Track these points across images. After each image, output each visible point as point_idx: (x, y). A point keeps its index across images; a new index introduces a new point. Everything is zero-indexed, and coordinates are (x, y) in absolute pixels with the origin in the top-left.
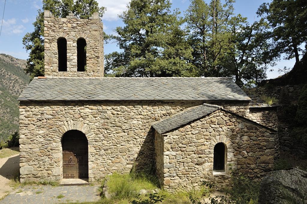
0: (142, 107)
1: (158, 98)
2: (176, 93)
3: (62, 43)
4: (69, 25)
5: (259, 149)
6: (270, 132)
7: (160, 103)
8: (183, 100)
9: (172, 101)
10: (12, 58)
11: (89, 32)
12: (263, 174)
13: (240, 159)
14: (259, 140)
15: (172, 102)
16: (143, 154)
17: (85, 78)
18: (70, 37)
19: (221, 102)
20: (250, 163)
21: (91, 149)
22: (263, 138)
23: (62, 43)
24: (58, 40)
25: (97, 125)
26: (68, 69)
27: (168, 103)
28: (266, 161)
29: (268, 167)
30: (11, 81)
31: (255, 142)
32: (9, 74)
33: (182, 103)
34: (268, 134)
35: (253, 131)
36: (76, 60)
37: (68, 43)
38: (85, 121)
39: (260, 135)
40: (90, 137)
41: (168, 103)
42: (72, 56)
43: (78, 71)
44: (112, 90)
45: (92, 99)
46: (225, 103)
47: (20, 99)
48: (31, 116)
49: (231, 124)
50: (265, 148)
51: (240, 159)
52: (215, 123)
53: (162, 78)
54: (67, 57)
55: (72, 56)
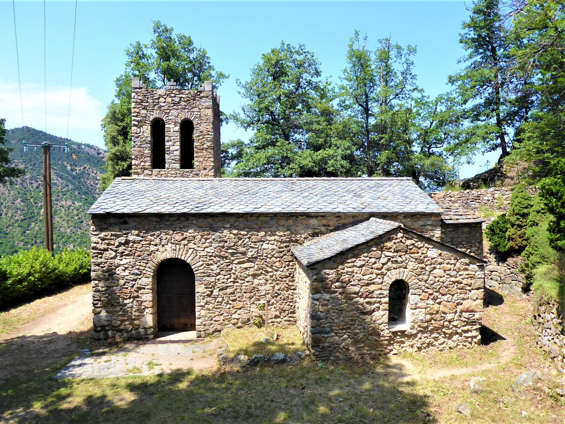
0: (277, 223)
1: (301, 209)
2: (328, 202)
3: (158, 127)
4: (169, 100)
5: (460, 289)
6: (478, 264)
7: (305, 217)
8: (339, 213)
9: (323, 214)
10: (98, 150)
11: (198, 110)
12: (465, 328)
13: (429, 306)
14: (460, 275)
15: (323, 216)
16: (280, 295)
17: (191, 179)
18: (170, 118)
19: (397, 215)
20: (446, 311)
21: (200, 288)
22: (467, 272)
23: (158, 127)
24: (152, 121)
25: (209, 251)
26: (167, 166)
27: (317, 217)
28: (471, 309)
29: (474, 318)
30: (97, 182)
31: (453, 279)
32: (95, 172)
33: (339, 216)
34: (475, 266)
35: (451, 262)
36: (178, 153)
37: (166, 126)
38: (194, 249)
39: (462, 268)
40: (197, 265)
41: (317, 217)
42: (173, 146)
43: (181, 168)
44: (231, 198)
45: (201, 212)
46: (404, 216)
47: (93, 210)
48: (109, 237)
49: (416, 252)
50: (470, 288)
51: (429, 306)
52: (390, 250)
53: (306, 178)
54: (166, 147)
55: (173, 146)
